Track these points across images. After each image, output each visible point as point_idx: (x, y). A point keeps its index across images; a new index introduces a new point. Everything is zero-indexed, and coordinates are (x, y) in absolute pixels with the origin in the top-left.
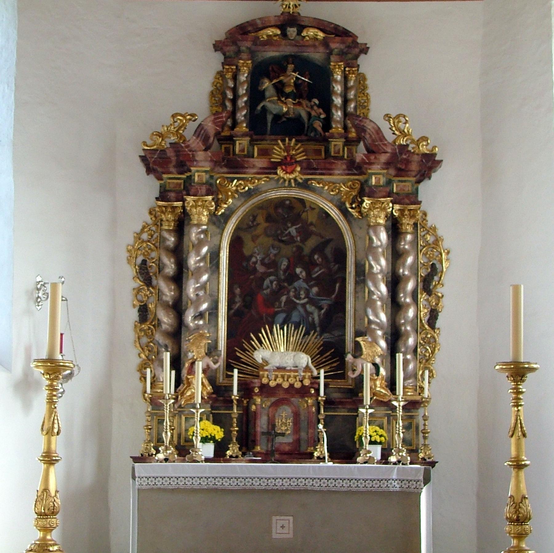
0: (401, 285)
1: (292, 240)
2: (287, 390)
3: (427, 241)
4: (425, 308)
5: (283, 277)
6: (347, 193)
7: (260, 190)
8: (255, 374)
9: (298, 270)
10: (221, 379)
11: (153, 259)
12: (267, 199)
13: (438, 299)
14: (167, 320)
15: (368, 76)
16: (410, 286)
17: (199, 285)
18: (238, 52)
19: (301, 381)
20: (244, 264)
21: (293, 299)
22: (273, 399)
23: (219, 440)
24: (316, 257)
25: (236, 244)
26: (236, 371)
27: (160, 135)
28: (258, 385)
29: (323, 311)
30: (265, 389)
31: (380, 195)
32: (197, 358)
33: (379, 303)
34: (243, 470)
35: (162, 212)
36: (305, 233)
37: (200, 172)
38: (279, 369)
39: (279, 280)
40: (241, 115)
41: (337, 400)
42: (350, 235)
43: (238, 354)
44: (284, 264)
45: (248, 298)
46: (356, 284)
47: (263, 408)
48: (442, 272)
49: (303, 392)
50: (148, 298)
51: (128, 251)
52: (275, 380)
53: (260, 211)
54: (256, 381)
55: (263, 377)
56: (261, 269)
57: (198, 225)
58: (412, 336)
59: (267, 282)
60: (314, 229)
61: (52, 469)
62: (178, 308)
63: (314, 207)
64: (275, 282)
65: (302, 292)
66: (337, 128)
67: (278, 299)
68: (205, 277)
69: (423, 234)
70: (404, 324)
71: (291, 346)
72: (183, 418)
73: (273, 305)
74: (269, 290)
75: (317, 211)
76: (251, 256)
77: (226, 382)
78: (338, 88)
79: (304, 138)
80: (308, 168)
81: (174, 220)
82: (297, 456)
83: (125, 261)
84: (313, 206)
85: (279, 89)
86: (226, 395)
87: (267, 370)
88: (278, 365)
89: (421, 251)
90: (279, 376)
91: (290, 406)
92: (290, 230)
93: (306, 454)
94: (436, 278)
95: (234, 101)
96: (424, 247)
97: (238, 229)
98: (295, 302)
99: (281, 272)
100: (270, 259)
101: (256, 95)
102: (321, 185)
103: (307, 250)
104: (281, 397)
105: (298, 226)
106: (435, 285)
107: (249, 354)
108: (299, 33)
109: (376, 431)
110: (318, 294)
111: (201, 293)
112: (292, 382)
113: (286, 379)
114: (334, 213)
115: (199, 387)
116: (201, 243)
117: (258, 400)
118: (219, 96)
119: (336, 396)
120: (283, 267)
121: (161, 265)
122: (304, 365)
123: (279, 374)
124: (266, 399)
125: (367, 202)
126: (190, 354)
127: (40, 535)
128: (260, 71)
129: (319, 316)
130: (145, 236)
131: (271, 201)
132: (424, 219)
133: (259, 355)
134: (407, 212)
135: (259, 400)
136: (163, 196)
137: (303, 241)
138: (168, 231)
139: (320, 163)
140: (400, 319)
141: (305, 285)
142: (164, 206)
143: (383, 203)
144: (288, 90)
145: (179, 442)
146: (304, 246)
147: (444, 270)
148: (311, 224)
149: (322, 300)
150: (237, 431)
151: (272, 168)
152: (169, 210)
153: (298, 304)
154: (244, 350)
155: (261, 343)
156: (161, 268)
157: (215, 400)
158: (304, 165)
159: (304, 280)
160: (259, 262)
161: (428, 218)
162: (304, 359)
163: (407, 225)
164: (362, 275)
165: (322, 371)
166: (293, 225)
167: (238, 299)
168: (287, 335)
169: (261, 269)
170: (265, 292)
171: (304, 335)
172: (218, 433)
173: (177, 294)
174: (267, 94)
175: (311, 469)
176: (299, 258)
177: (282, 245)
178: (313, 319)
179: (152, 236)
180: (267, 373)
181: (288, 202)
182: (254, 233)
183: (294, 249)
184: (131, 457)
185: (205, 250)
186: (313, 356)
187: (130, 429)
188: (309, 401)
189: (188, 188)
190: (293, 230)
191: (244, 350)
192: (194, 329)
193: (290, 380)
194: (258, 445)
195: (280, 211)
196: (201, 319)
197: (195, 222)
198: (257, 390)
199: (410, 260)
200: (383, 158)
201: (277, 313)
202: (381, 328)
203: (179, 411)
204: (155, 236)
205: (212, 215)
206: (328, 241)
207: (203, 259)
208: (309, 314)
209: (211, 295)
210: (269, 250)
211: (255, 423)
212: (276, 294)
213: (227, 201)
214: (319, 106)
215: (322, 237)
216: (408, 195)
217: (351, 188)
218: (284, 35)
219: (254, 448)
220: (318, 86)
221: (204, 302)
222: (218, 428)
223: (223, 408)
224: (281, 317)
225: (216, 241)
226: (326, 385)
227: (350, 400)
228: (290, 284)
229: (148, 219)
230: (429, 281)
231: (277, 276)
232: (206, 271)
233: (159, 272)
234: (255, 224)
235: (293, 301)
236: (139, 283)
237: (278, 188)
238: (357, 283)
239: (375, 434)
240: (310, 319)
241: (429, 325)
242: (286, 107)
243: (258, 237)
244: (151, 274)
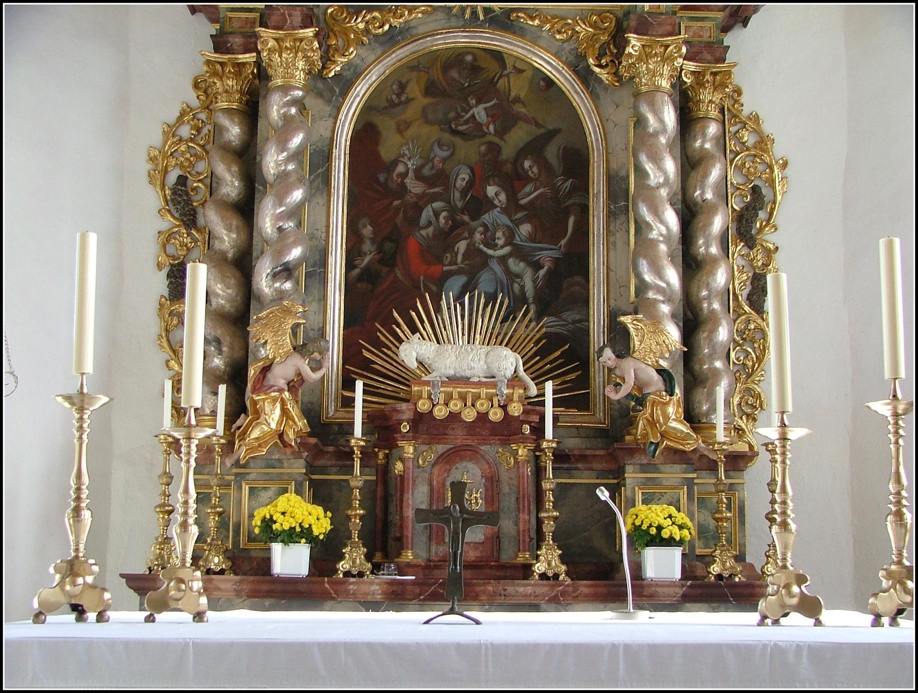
0: (700, 221)
1: (478, 130)
2: (471, 427)
3: (744, 143)
4: (741, 272)
5: (459, 204)
7: (414, 31)
8: (402, 395)
9: (491, 190)
10: (331, 410)
11: (199, 174)
12: (427, 51)
13: (769, 254)
16: (718, 223)
17: (283, 209)
19: (504, 407)
20: (382, 178)
21: (481, 246)
22: (441, 448)
23: (321, 537)
24: (527, 164)
25: (365, 136)
26: (359, 385)
28: (408, 415)
29: (542, 272)
30: (421, 421)
31: (661, 30)
32: (274, 358)
33: (663, 247)
35: (215, 74)
36: (506, 118)
38: (453, 380)
39: (452, 211)
41: (576, 452)
42: (596, 119)
43: (366, 354)
44: (463, 177)
45: (388, 246)
46: (608, 217)
47: (419, 467)
48: (774, 202)
49: (506, 431)
50: (188, 249)
51: (151, 159)
52: (446, 404)
53: (415, 74)
54: (404, 406)
55: (420, 397)
56: (415, 187)
57: (285, 89)
58: (724, 323)
59: (427, 214)
60: (523, 110)
63: (522, 68)
64: (444, 214)
65: (499, 234)
67: (450, 248)
68: (297, 195)
69: (733, 129)
70: (708, 298)
71: (478, 336)
72: (246, 489)
73: (440, 261)
74: (430, 230)
75: (529, 73)
76: (395, 163)
77: (342, 414)
81: (241, 92)
82: (494, 572)
83: (145, 179)
84: (519, 65)
86: (342, 441)
87: (427, 383)
88: (451, 372)
89: (732, 161)
90: (455, 396)
91: (477, 463)
92: (475, 110)
93: (514, 567)
94: (762, 215)
96: (737, 154)
97: (368, 109)
98: (485, 253)
99: (457, 195)
100: (433, 167)
102: (537, 22)
103: (508, 151)
104: (459, 442)
105: (488, 105)
106: (761, 230)
107: (389, 352)
109: (670, 516)
110: (532, 238)
111: (290, 225)
112: (483, 409)
113: (469, 403)
116: (288, 126)
117: (409, 450)
119: (572, 443)
120: (460, 184)
122: (509, 373)
123: (456, 391)
124: (424, 447)
129: (534, 281)
130: (185, 131)
131: (434, 56)
132: (736, 101)
133: (413, 351)
134: (708, 77)
135: (411, 449)
136: (220, 44)
137: (502, 133)
138: (228, 111)
140: (699, 291)
141: (505, 220)
142: (219, 63)
143: (667, 47)
145: (236, 543)
146: (502, 143)
147: (779, 198)
148: (517, 100)
149: (542, 249)
150: (362, 518)
152: (229, 68)
153: (491, 257)
154: (379, 345)
157: (317, 452)
159: (505, 211)
160: (411, 174)
161: (744, 99)
162: (508, 361)
163: (708, 100)
164: (620, 199)
165: (549, 386)
166: (479, 102)
167: (367, 246)
168: (470, 315)
169: (415, 187)
170: (423, 232)
171: (504, 320)
172: (320, 522)
173: (243, 236)
175: (805, 653)
176: (492, 166)
177: (458, 140)
178: (522, 288)
179: (199, 130)
180: (427, 388)
181: (469, 58)
182: (403, 117)
183: (483, 148)
184: (122, 576)
185: (296, 141)
186: (527, 357)
188: (520, 452)
190: (480, 112)
191: (379, 345)
192: (274, 300)
193: (478, 404)
194: (407, 549)
195: (454, 74)
196: (288, 278)
197: (279, 82)
198: (405, 428)
199: (715, 173)
201: (448, 275)
202: (669, 300)
203: (237, 475)
204: (205, 131)
205: (316, 76)
206: (551, 135)
207: (296, 156)
208: (513, 277)
209: (312, 237)
210: (432, 149)
211: (402, 501)
212: (446, 238)
213: (347, 50)
215: (537, 125)
216: (709, 46)
217: (593, 25)
219: (399, 555)
221: (295, 244)
222: (320, 510)
223: (334, 469)
225: (323, 128)
226: (556, 419)
227: (601, 452)
228: (475, 216)
229: (192, 98)
230: (746, 227)
231: (449, 203)
232: (300, 181)
233: (211, 195)
234: (403, 99)
235: (481, 251)
236: (167, 222)
237: (450, 29)
238: (611, 215)
239: (669, 521)
240: (516, 287)
241: (751, 305)
243: (408, 125)
244: (195, 204)
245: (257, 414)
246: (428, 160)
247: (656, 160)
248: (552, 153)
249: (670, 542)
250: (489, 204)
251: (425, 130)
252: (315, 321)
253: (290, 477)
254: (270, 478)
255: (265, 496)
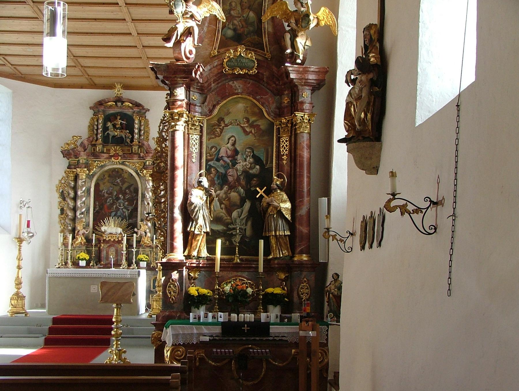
6: (138, 167)
9: (120, 196)
14: (70, 214)
15: (150, 120)
18: (99, 111)
22: (108, 245)
25: (97, 186)
27: (68, 144)
30: (104, 240)
34: (96, 271)
36: (123, 182)
37: (82, 159)
39: (113, 200)
40: (99, 136)
56: (106, 195)
57: (82, 179)
59: (108, 200)
61: (20, 271)
62: (75, 209)
63: (127, 172)
66: (136, 141)
67: (113, 207)
68: (84, 199)
73: (110, 209)
78: (136, 126)
79: (123, 145)
80: (123, 157)
85: (114, 126)
95: (97, 130)
97: (97, 180)
101: (105, 129)
108: (122, 104)
111: (83, 205)
114: (134, 174)
115: (80, 239)
116: (83, 186)
118: (91, 127)
121: (68, 193)
125: (145, 171)
126: (262, 127)
127: (16, 290)
128: (108, 118)
130: (63, 181)
133: (103, 229)
136: (69, 167)
137: (122, 185)
139: (129, 155)
141: (123, 201)
144: (117, 126)
151: (111, 156)
154: (99, 226)
155: (105, 223)
156: (69, 194)
158: (122, 156)
159: (123, 200)
162: (120, 230)
167: (97, 206)
169: (106, 195)
172: (87, 257)
174: (109, 128)
176: (121, 191)
185: (84, 189)
187: (56, 255)
189: (77, 165)
190: (118, 180)
200: (151, 155)
201: (112, 212)
207: (84, 192)
212: (112, 205)
214: (129, 133)
218: (116, 104)
220: (129, 127)
224: (113, 214)
229: (64, 175)
242: (117, 133)
245: (77, 239)
246: (109, 190)
247: (148, 193)
248: (132, 189)
249: (144, 261)
250: (119, 198)
251: (108, 184)
252: (88, 221)
253: (82, 249)
254: (79, 250)
255: (78, 253)
